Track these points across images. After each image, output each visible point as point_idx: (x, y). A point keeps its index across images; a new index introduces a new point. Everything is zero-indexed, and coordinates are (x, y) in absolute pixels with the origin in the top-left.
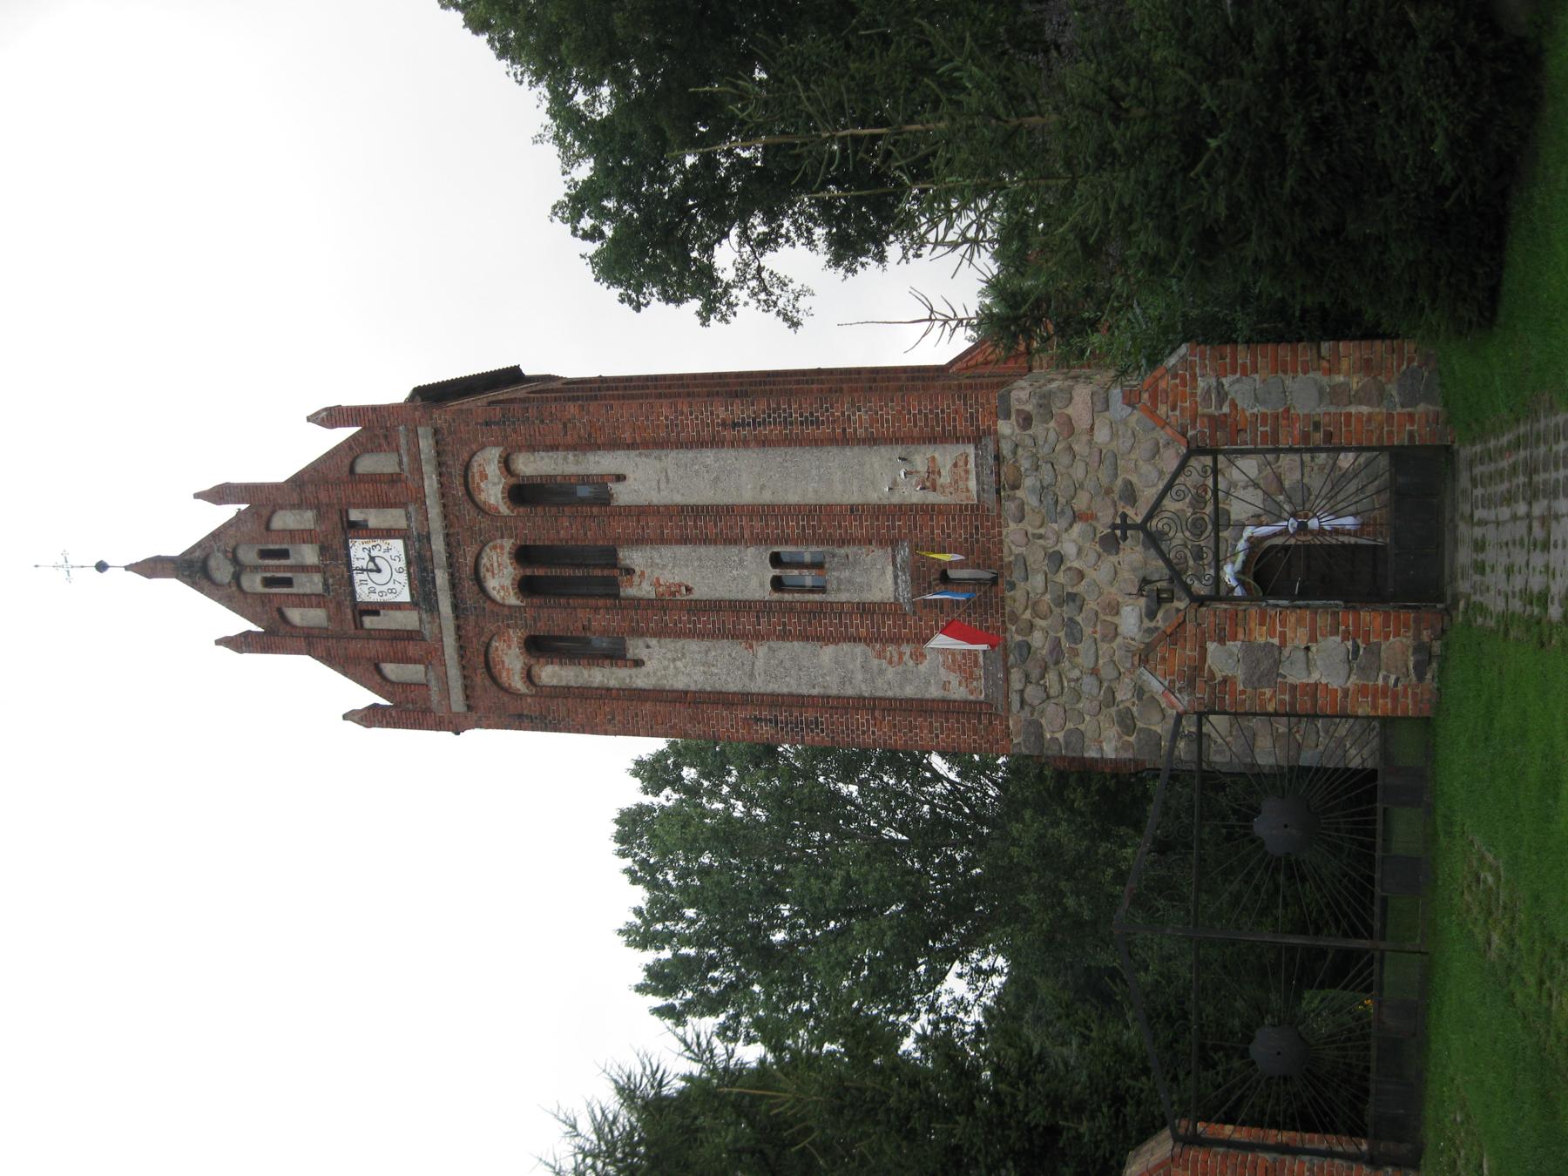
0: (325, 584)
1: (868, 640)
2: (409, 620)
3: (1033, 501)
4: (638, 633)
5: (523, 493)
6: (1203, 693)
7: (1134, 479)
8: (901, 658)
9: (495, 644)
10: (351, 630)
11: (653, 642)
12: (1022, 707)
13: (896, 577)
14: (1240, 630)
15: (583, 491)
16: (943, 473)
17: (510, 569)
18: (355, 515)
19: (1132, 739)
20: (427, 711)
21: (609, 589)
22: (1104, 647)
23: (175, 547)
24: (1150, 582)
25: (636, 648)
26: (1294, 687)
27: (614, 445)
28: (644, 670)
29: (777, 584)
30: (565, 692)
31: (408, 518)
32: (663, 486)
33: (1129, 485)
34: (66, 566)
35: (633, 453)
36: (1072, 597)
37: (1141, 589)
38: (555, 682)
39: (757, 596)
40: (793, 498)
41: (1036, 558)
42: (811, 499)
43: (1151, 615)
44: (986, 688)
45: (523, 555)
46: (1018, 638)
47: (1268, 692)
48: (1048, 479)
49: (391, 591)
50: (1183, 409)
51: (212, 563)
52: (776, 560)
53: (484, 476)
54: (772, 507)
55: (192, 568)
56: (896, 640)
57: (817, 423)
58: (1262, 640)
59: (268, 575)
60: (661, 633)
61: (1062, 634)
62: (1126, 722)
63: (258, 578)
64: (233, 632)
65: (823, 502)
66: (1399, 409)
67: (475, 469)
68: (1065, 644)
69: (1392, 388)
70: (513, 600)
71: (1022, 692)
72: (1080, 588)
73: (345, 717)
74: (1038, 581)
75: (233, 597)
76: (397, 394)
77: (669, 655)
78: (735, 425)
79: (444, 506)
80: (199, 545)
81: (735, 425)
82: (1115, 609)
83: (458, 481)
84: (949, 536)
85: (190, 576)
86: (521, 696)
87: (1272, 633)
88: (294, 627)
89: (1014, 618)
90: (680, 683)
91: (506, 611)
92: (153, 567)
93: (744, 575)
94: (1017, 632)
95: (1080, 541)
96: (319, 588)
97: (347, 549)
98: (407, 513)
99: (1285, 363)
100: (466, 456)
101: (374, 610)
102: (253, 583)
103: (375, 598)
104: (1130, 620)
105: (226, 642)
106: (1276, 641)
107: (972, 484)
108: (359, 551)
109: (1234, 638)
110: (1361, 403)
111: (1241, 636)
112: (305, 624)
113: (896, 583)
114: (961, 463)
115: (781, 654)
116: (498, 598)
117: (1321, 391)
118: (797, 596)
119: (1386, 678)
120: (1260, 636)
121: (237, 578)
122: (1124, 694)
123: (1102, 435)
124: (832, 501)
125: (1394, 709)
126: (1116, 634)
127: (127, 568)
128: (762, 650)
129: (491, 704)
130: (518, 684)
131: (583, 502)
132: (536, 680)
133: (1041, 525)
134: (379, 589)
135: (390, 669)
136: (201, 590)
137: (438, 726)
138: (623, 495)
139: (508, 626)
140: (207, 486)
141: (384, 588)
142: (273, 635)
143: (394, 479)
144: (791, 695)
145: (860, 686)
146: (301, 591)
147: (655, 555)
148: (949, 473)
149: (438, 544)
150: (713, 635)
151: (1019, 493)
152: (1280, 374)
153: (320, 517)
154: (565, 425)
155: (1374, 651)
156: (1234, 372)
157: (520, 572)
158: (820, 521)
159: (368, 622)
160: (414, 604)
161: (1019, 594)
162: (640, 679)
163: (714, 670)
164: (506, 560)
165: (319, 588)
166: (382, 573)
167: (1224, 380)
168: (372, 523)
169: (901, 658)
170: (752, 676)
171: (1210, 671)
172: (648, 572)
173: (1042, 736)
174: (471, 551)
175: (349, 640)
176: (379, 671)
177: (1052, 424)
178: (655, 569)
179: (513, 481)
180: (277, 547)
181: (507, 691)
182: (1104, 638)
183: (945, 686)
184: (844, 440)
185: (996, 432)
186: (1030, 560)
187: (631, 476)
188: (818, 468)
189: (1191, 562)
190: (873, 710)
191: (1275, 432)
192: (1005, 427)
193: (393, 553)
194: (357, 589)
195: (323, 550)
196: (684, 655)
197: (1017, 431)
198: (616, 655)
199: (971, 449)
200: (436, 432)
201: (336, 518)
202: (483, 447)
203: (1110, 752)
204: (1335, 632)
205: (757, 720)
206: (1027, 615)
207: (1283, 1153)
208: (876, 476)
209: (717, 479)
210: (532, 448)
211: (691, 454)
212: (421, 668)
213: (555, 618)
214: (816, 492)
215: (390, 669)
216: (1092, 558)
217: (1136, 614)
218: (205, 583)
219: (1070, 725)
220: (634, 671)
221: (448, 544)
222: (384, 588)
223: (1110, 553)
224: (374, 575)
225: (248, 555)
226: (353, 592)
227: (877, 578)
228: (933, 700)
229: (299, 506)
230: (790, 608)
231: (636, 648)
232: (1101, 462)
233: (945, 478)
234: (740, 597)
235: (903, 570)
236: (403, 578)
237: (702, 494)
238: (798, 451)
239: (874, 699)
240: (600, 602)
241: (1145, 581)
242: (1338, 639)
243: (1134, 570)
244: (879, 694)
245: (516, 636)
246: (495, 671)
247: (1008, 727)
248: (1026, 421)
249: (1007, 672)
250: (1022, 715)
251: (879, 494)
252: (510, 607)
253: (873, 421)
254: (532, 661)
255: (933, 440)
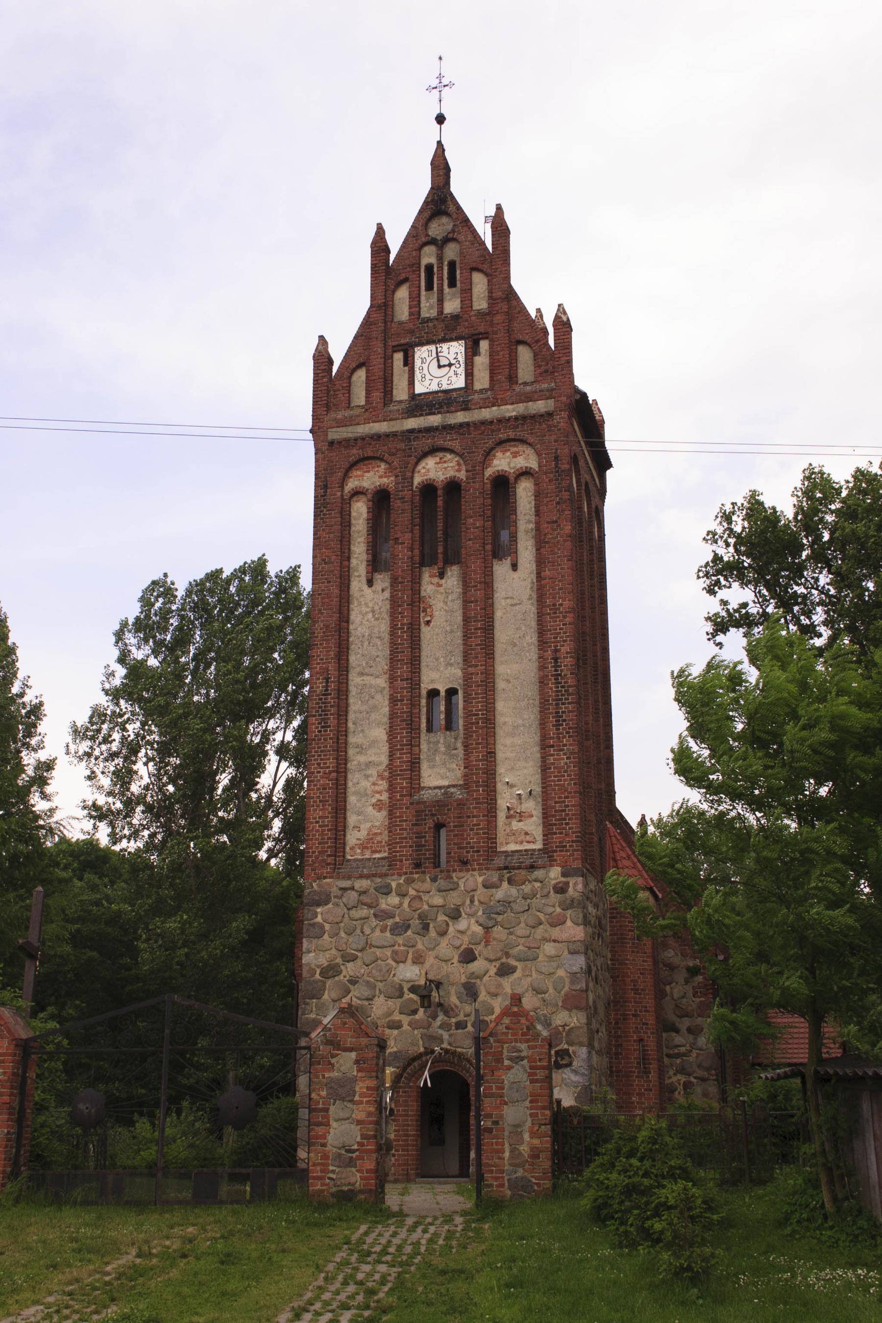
0: (429, 320)
1: (390, 767)
2: (400, 393)
3: (500, 894)
4: (394, 582)
5: (503, 486)
6: (324, 1050)
7: (518, 974)
8: (378, 792)
9: (383, 466)
10: (391, 343)
11: (387, 594)
12: (341, 889)
13: (440, 788)
14: (363, 1074)
15: (504, 535)
16: (521, 824)
17: (442, 478)
18: (484, 345)
19: (317, 976)
20: (328, 408)
21: (426, 559)
22: (388, 952)
23: (456, 188)
24: (438, 988)
25: (382, 581)
26: (327, 1110)
27: (540, 562)
28: (365, 587)
29: (433, 694)
30: (346, 523)
31: (481, 391)
32: (509, 601)
33: (513, 970)
34: (441, 86)
35: (534, 577)
36: (426, 927)
37: (431, 981)
38: (354, 514)
39: (424, 678)
40: (500, 706)
41: (454, 898)
42: (500, 720)
43: (413, 989)
44: (356, 860)
45: (453, 487)
46: (394, 885)
47: (324, 1093)
48: (516, 907)
49: (423, 377)
50: (506, 1034)
51: (444, 220)
52: (451, 692)
53: (515, 455)
54: (493, 689)
55: (440, 202)
56: (391, 789)
57: (557, 725)
58: (357, 1089)
59: (435, 270)
60: (394, 602)
61: (397, 919)
62: (330, 971)
63: (433, 260)
64: (389, 238)
65: (498, 730)
66: (506, 1178)
67: (521, 448)
68: (390, 922)
69: (520, 1173)
70: (417, 480)
71: (353, 888)
72: (433, 933)
73: (322, 338)
74: (438, 900)
75: (418, 236)
76: (585, 378)
77: (376, 608)
78: (556, 660)
79: (492, 422)
80: (459, 208)
81: (556, 660)
82: (418, 960)
83: (511, 434)
84: (472, 830)
85: (432, 200)
86: (342, 487)
87: (361, 1095)
88: (394, 292)
89: (410, 881)
90: (355, 616)
91: (409, 474)
92: (440, 167)
93: (440, 670)
94: (399, 885)
95: (469, 933)
96: (425, 314)
97: (457, 339)
98: (486, 390)
99: (537, 1101)
100: (531, 440)
101: (409, 361)
102: (429, 256)
103: (418, 363)
104: (410, 973)
105: (380, 232)
106: (357, 1098)
107: (512, 847)
108: (455, 350)
109: (358, 1071)
110: (511, 1152)
111: (360, 1074)
112: (396, 302)
113: (435, 788)
114: (528, 838)
115: (379, 697)
116: (419, 467)
117: (518, 1126)
118: (424, 710)
119: (333, 1172)
120: (360, 1087)
121: (433, 242)
122: (349, 970)
123: (549, 949)
124: (497, 737)
125: (314, 1178)
126: (397, 962)
127: (439, 143)
128: (382, 682)
129: (335, 460)
130: (352, 484)
131: (496, 536)
132: (355, 499)
133: (481, 903)
134: (425, 366)
135: (361, 375)
136: (421, 212)
137: (316, 417)
138: (501, 569)
139: (397, 476)
140: (508, 218)
141: (425, 371)
142: (386, 272)
143: (512, 378)
144: (347, 705)
145: (355, 759)
146: (423, 298)
147: (455, 596)
148: (522, 828)
149: (460, 417)
150: (393, 644)
151: (505, 884)
152: (529, 1099)
153: (481, 314)
154: (556, 522)
155: (351, 1163)
156: (531, 1068)
157: (440, 485)
158: (482, 728)
159: (399, 357)
160: (413, 396)
161: (427, 885)
162: (358, 584)
163: (366, 644)
164: (451, 473)
165: (425, 314)
166: (439, 368)
167: (525, 1061)
168: (478, 360)
169: (378, 792)
170: (362, 674)
171: (337, 1055)
172: (441, 589)
173: (318, 905)
174: (456, 445)
175: (385, 338)
176: (359, 366)
177: (558, 910)
178: (443, 593)
179: (512, 479)
180: (458, 277)
181: (346, 476)
182: (395, 953)
183: (357, 828)
184: (544, 746)
185: (551, 866)
186: (454, 894)
187: (515, 575)
188: (524, 725)
189: (453, 1020)
190: (337, 772)
191: (492, 1096)
192: (555, 873)
193: (454, 379)
194: (425, 348)
195: (455, 318)
196: (377, 619)
197: (553, 882)
198: (375, 565)
199: (539, 846)
200: (550, 414)
201: (482, 329)
202: (539, 454)
203: (308, 959)
204: (363, 1137)
205: (327, 680)
206: (412, 892)
207: (19, 1113)
208: (518, 773)
209: (515, 645)
210: (538, 495)
211: (534, 624)
212: (363, 403)
213: (403, 515)
214: (505, 723)
215: (361, 375)
216: (457, 943)
217: (414, 977)
218: (427, 215)
219: (327, 927)
220: (364, 580)
221: (461, 425)
222: (425, 371)
223: (459, 957)
224: (435, 363)
225: (451, 252)
226: (422, 344)
227: (440, 773)
228: (345, 818)
229: (491, 298)
230: (414, 703)
231: (382, 581)
232: (529, 948)
233: (516, 825)
234: (423, 664)
235: (446, 793)
236: (434, 387)
237: (503, 634)
238: (536, 710)
239: (346, 772)
240: (417, 552)
241: (439, 985)
242: (358, 1139)
243: (448, 976)
244: (350, 776)
245: (388, 481)
246: (361, 465)
247: (325, 878)
248: (561, 889)
249: (367, 877)
250: (335, 889)
251: (505, 774)
252: (412, 478)
253: (559, 769)
254: (370, 496)
255: (545, 816)
